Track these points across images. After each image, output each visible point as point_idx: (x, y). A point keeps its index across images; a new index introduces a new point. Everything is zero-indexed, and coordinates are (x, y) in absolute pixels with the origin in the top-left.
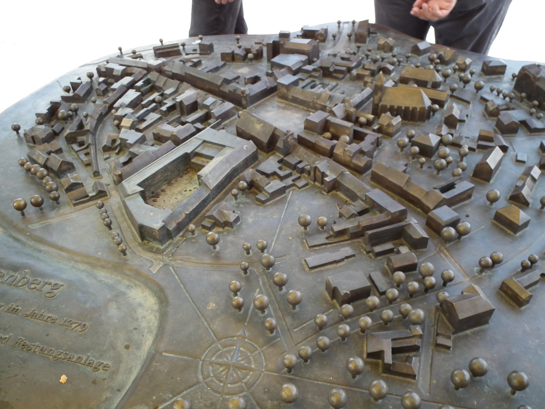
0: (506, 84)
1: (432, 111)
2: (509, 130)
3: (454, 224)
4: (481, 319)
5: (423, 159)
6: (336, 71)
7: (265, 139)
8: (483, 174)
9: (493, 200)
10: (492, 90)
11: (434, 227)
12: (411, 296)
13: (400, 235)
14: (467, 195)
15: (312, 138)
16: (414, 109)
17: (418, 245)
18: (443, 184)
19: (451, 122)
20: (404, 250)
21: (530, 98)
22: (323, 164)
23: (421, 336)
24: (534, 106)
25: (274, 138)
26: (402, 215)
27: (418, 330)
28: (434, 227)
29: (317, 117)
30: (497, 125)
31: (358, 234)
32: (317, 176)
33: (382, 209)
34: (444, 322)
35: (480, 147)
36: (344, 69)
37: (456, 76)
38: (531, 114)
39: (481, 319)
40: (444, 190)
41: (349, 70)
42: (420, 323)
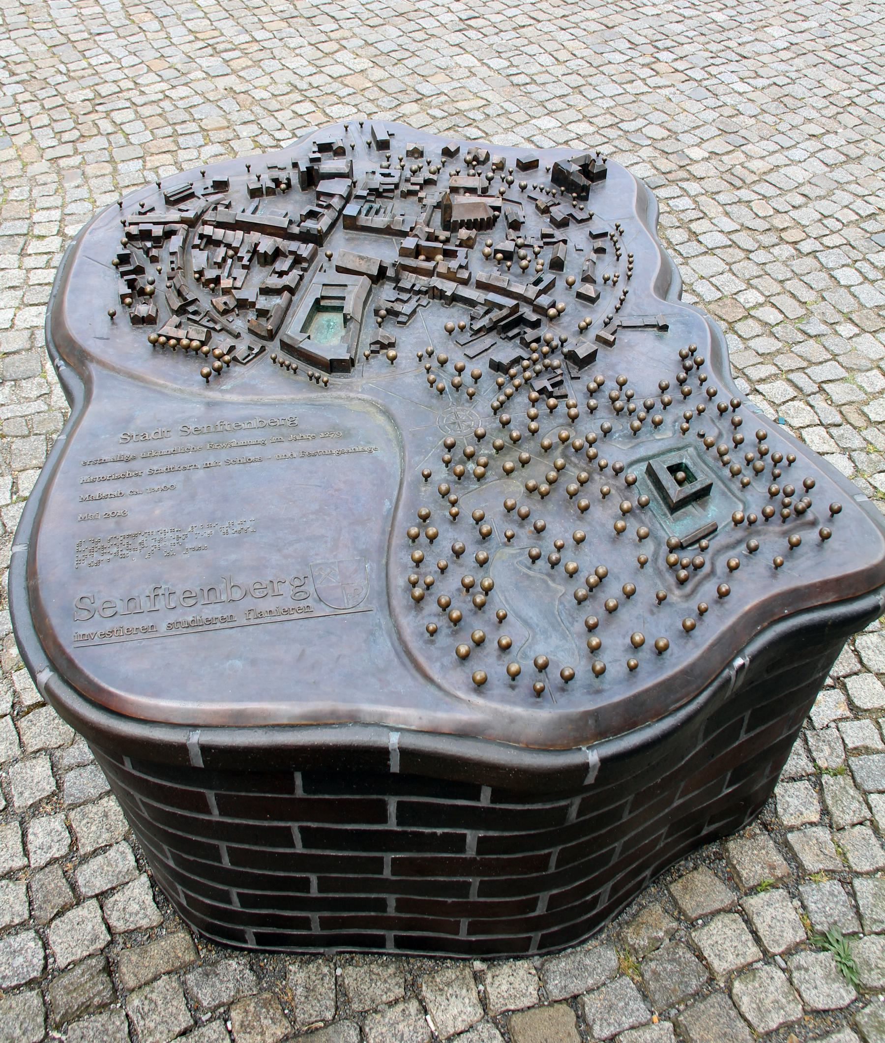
0: (542, 178)
1: (496, 218)
2: (563, 224)
3: (553, 305)
4: (591, 358)
5: (509, 263)
6: (385, 191)
7: (375, 272)
8: (557, 265)
9: (570, 285)
10: (535, 188)
11: (538, 309)
12: (545, 356)
13: (521, 321)
14: (552, 285)
15: (411, 262)
16: (482, 220)
17: (536, 325)
18: (533, 279)
19: (515, 225)
20: (528, 330)
21: (569, 190)
22: (436, 282)
23: (562, 374)
24: (574, 199)
25: (382, 270)
26: (515, 309)
27: (559, 371)
28: (538, 309)
29: (410, 243)
30: (551, 221)
31: (488, 330)
32: (436, 294)
33: (501, 307)
34: (413, 956)
35: (546, 244)
36: (393, 187)
37: (497, 177)
38: (574, 206)
39: (591, 358)
40: (536, 283)
41: (397, 186)
42: (559, 367)
